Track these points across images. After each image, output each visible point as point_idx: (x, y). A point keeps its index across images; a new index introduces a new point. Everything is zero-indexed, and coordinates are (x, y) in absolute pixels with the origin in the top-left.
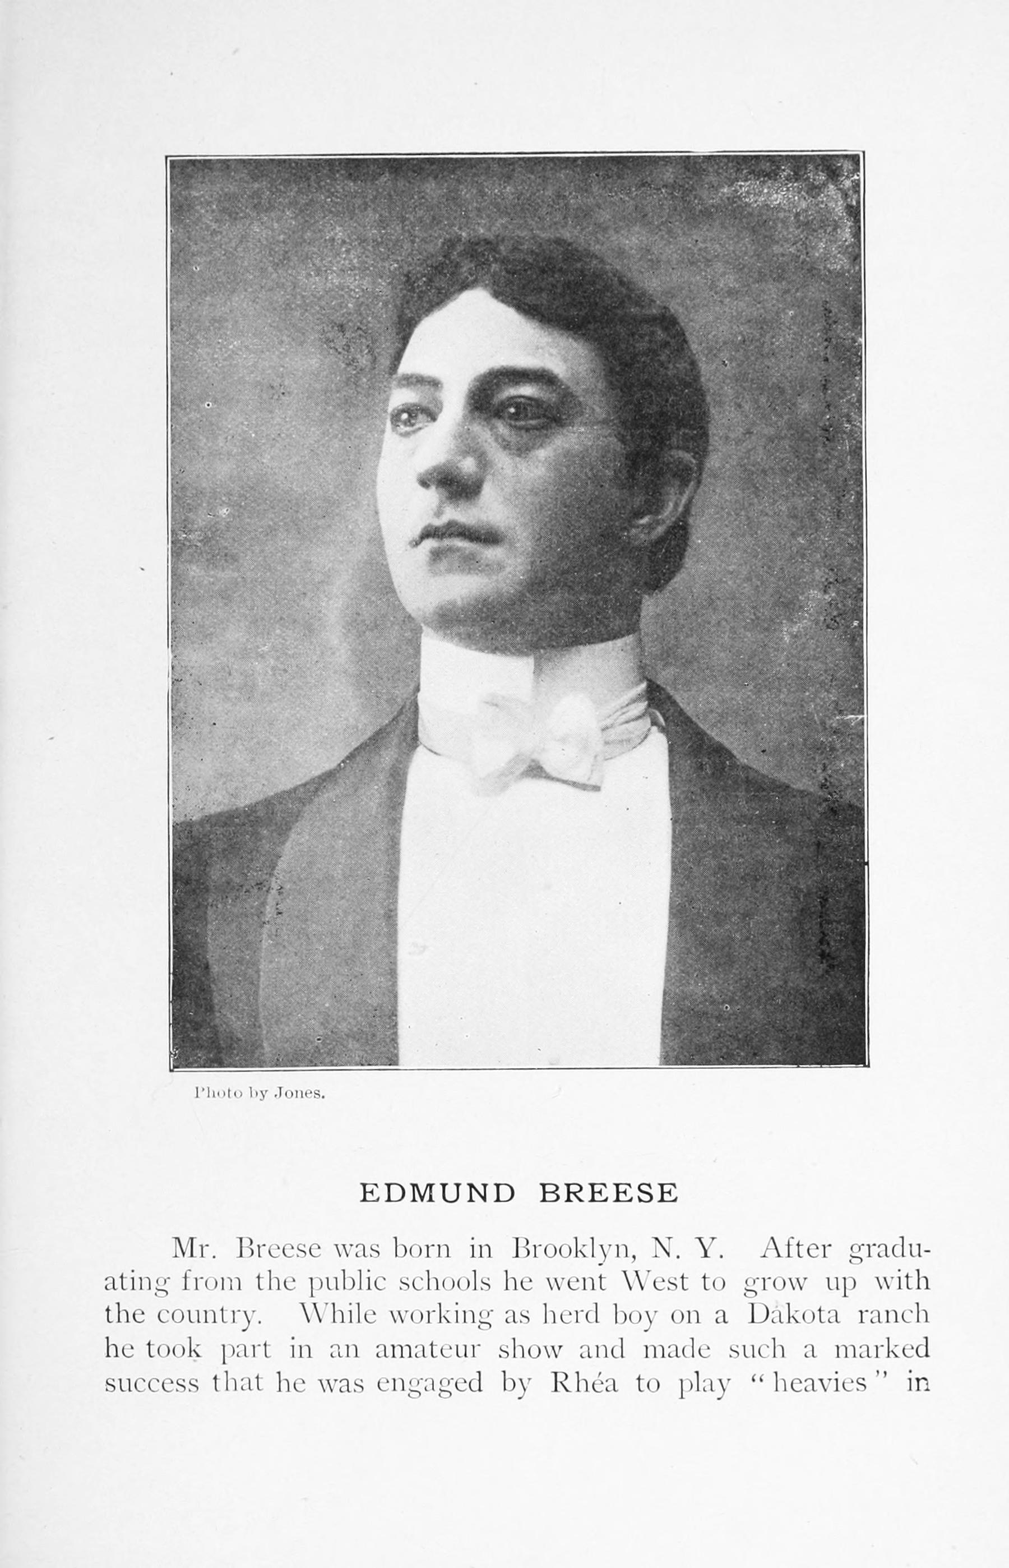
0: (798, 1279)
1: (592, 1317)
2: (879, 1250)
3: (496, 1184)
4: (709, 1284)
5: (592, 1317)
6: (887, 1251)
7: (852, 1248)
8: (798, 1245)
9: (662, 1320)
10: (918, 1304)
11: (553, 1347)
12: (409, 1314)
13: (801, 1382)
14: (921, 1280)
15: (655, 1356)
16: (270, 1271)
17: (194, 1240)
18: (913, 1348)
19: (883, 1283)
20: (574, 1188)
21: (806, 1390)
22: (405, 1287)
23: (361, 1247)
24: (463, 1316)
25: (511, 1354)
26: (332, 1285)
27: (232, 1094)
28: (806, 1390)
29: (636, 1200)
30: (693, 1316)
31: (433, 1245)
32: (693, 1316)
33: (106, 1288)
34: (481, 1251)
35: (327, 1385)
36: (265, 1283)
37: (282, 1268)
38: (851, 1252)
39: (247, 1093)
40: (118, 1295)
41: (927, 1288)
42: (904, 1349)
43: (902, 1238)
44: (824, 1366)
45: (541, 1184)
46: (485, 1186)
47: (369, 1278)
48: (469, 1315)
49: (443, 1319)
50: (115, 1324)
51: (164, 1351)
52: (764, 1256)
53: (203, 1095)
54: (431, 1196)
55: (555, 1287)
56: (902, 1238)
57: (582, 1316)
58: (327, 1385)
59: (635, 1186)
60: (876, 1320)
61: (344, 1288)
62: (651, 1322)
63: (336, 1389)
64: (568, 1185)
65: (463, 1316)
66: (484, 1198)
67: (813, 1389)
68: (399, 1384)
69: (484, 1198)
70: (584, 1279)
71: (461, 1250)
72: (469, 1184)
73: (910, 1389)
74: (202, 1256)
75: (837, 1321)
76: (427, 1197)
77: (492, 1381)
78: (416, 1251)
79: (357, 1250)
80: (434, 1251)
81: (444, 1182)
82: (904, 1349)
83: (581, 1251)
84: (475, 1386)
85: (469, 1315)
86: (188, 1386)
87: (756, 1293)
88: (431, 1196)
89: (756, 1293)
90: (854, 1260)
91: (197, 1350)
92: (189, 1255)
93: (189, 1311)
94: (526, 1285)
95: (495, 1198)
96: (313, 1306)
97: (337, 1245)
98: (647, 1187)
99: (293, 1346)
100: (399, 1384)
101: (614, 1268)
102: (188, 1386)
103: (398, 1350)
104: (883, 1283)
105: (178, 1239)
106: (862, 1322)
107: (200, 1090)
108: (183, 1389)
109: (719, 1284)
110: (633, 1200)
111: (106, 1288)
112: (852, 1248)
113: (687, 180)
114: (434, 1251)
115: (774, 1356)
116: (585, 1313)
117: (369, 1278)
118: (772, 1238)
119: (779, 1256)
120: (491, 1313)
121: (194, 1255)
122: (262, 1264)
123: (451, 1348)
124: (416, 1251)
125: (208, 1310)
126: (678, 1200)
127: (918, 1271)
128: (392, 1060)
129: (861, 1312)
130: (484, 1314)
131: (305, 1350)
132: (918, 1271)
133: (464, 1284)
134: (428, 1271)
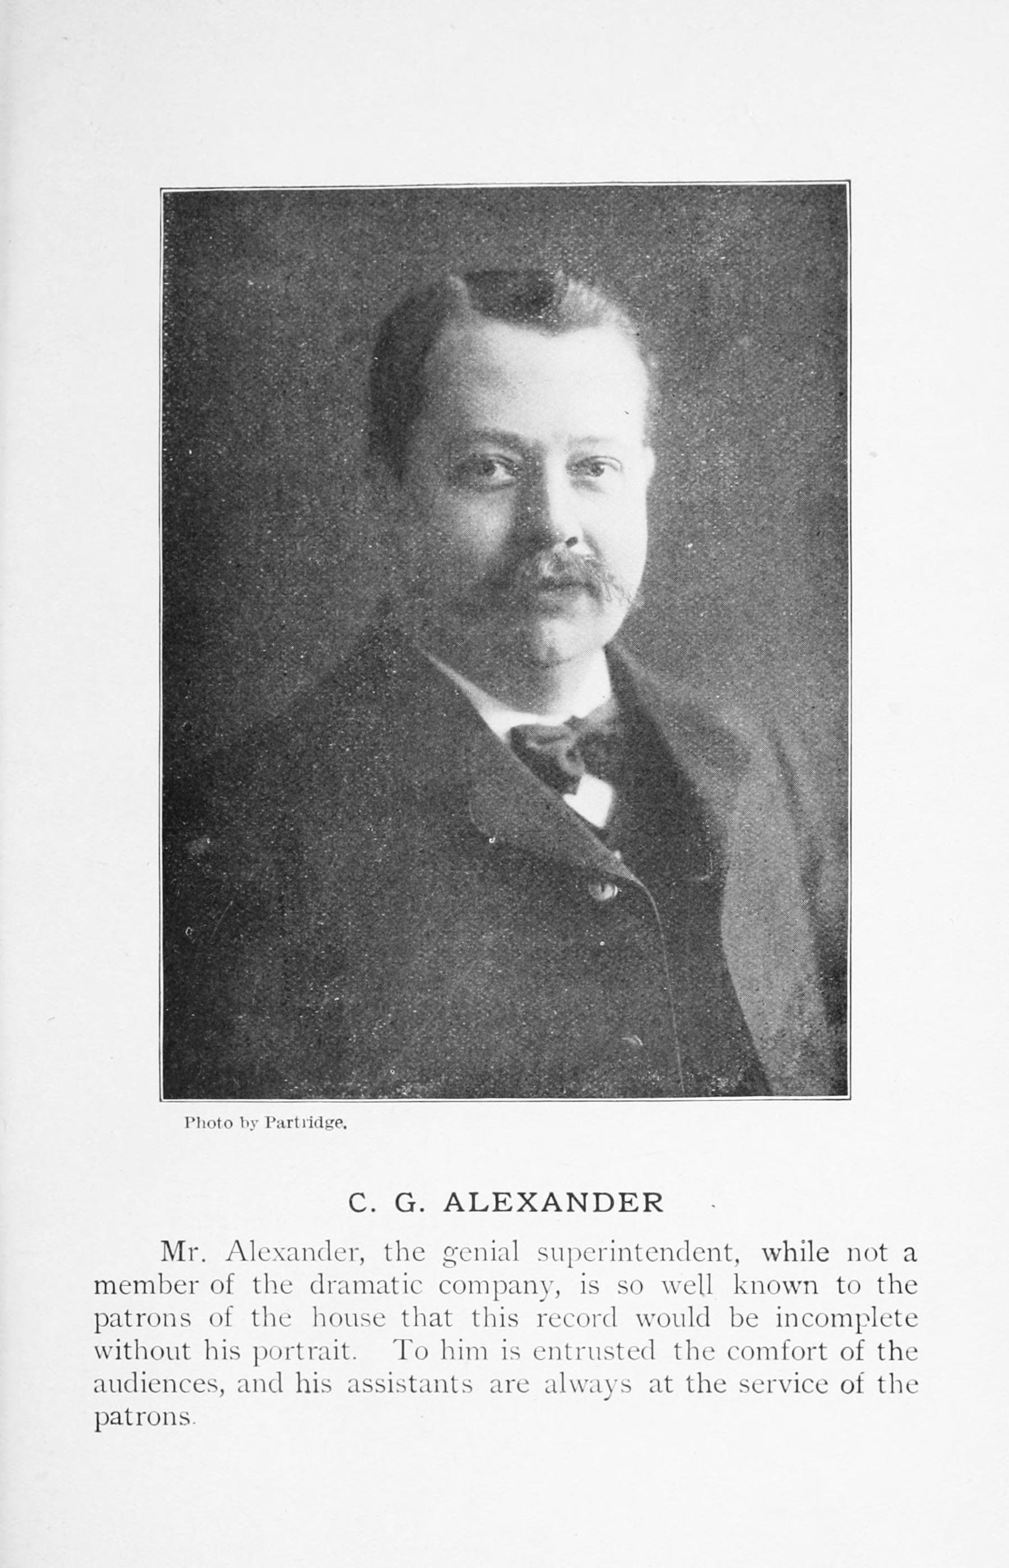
0: (672, 1282)
1: (609, 1320)
3: (595, 1194)
4: (844, 1288)
5: (609, 1320)
6: (675, 1256)
10: (265, 1307)
11: (646, 1316)
12: (656, 1318)
15: (145, 1292)
17: (183, 1244)
18: (638, 1350)
19: (670, 1287)
21: (421, 1391)
22: (623, 1290)
26: (679, 1322)
27: (222, 1123)
37: (280, 1272)
38: (444, 1256)
39: (237, 1123)
40: (263, 1299)
42: (629, 1352)
43: (687, 1242)
45: (494, 1193)
46: (585, 1195)
47: (406, 1282)
52: (229, 1260)
53: (193, 1125)
55: (671, 1291)
56: (687, 1242)
57: (599, 1320)
61: (161, 1292)
63: (587, 1390)
64: (623, 1195)
66: (584, 1208)
67: (103, 1390)
69: (584, 1208)
70: (165, 1381)
72: (568, 1194)
74: (191, 1259)
81: (584, 1192)
82: (629, 1352)
86: (375, 1387)
90: (448, 1264)
91: (743, 1287)
92: (178, 1258)
93: (675, 1315)
94: (286, 1288)
95: (595, 1208)
101: (722, 1273)
102: (375, 1387)
103: (473, 1352)
104: (670, 1287)
105: (166, 1242)
106: (403, 1358)
107: (190, 1120)
108: (369, 1388)
109: (854, 1287)
110: (513, 1209)
113: (208, 665)
115: (551, 1358)
116: (603, 1316)
117: (406, 1282)
118: (237, 1242)
119: (244, 1259)
122: (257, 1269)
125: (835, 1314)
128: (844, 1092)
129: (540, 1315)
134: (266, 1274)
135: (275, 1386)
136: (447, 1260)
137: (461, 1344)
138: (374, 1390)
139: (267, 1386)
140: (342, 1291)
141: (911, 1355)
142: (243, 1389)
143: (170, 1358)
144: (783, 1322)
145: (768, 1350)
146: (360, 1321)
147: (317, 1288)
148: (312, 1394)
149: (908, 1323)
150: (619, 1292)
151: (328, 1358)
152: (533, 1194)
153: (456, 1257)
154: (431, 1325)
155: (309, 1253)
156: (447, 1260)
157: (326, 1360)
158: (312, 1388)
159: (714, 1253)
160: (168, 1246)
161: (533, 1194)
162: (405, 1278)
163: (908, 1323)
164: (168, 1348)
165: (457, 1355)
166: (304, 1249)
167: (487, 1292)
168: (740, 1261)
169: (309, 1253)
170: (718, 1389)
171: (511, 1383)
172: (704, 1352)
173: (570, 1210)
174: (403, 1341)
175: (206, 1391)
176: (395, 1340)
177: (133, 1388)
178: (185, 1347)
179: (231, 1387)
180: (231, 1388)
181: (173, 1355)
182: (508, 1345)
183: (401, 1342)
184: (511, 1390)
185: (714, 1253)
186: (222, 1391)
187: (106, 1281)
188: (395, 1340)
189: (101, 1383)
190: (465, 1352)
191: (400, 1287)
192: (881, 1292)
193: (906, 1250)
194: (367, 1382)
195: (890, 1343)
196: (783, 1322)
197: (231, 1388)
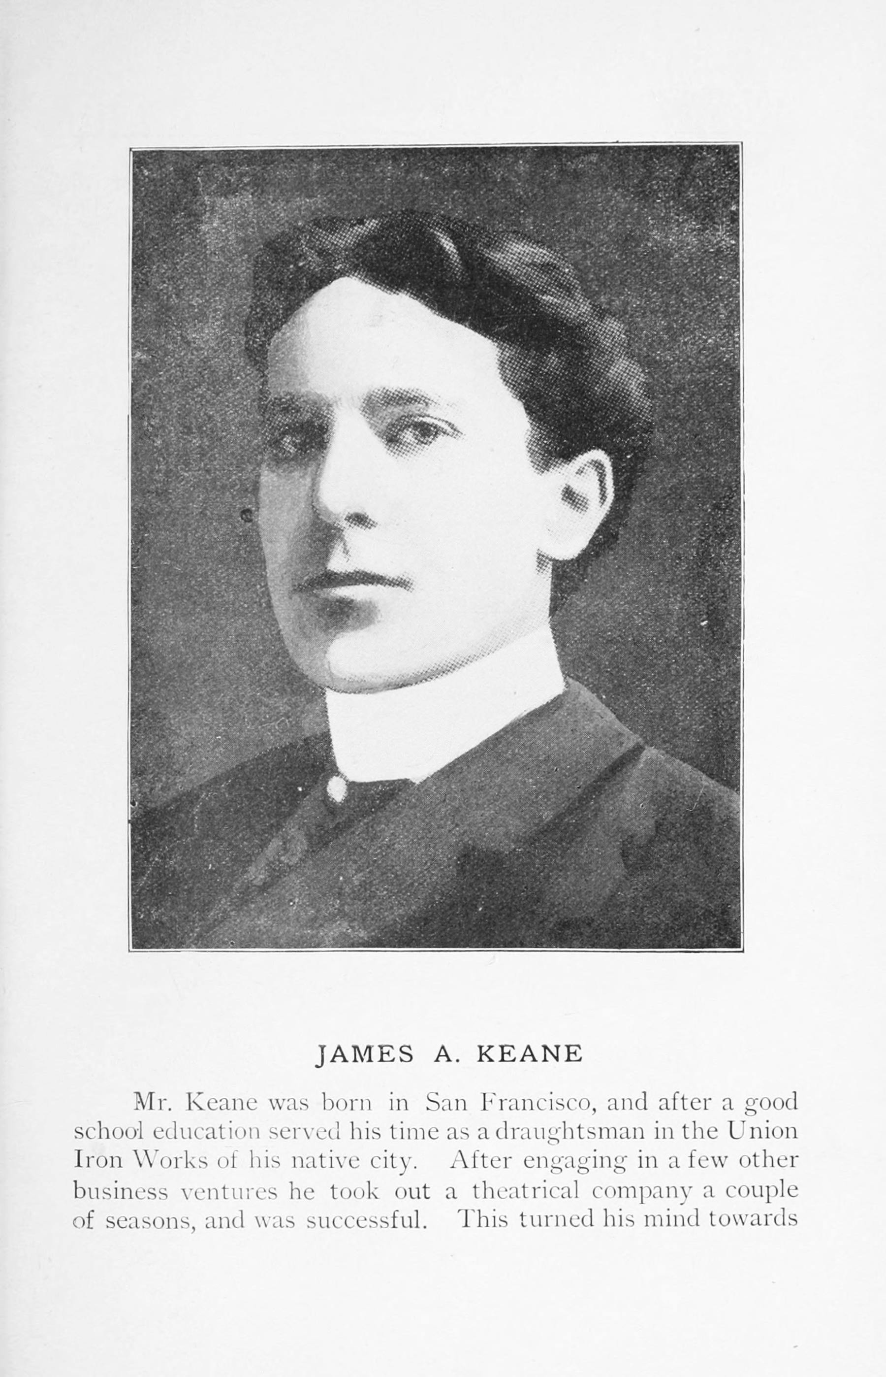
2: (510, 1104)
3: (379, 1046)
7: (747, 1102)
8: (683, 1099)
9: (516, 1164)
13: (506, 1190)
14: (102, 1131)
16: (694, 1122)
17: (153, 1095)
20: (385, 1050)
21: (130, 1227)
22: (79, 1136)
23: (292, 1101)
24: (600, 1162)
25: (113, 1195)
28: (130, 1227)
29: (397, 1060)
30: (791, 1132)
31: (357, 1100)
32: (791, 1132)
33: (449, 1138)
34: (401, 1104)
35: (262, 1222)
36: (690, 1132)
38: (746, 1105)
40: (764, 1143)
41: (642, 1138)
43: (645, 1093)
44: (723, 1206)
45: (320, 1046)
46: (557, 1047)
48: (606, 1161)
49: (189, 1165)
50: (761, 1168)
51: (346, 1193)
54: (370, 1057)
56: (645, 1093)
58: (262, 1222)
59: (397, 1048)
60: (525, 1136)
62: (406, 1167)
63: (270, 1225)
65: (600, 1162)
66: (557, 1058)
68: (543, 1161)
69: (557, 1058)
71: (381, 1104)
73: (606, 1225)
75: (314, 1166)
76: (366, 1058)
77: (249, 1221)
78: (342, 1105)
79: (289, 1103)
80: (357, 1104)
82: (700, 1160)
83: (194, 1102)
84: (587, 1221)
85: (606, 1161)
86: (158, 1195)
87: (558, 1141)
88: (370, 1057)
89: (558, 1141)
90: (749, 1112)
92: (149, 1108)
96: (144, 1153)
97: (271, 1100)
98: (408, 1049)
99: (116, 1189)
100: (543, 1161)
102: (380, 1223)
105: (138, 1093)
106: (466, 1225)
111: (449, 1138)
112: (747, 1102)
114: (357, 1104)
120: (625, 1159)
121: (153, 1108)
123: (204, 1191)
124: (342, 1105)
126: (582, 1060)
127: (100, 1122)
130: (619, 1160)
131: (651, 1161)
132: (100, 1122)
133: (131, 1133)
135: (238, 1222)
136: (748, 1110)
137: (595, 1154)
138: (379, 1226)
139: (231, 1223)
140: (209, 1136)
141: (309, 1195)
142: (210, 1225)
143: (755, 1196)
144: (644, 1164)
145: (608, 1130)
146: (597, 1132)
147: (502, 1134)
148: (414, 1229)
149: (350, 1165)
150: (76, 1137)
151: (660, 1196)
152: (490, 1047)
153: (756, 1107)
154: (307, 1167)
155: (238, 1103)
156: (748, 1110)
157: (711, 1198)
158: (491, 1223)
159: (213, 1193)
160: (140, 1096)
161: (490, 1047)
162: (231, 1125)
163: (350, 1165)
164: (410, 1189)
165: (665, 1222)
166: (160, 1100)
167: (258, 1137)
168: (597, 1110)
169: (238, 1103)
170: (360, 1225)
171: (769, 1218)
172: (305, 1192)
173: (545, 1060)
174: (466, 1211)
175: (368, 1226)
176: (459, 1210)
177: (240, 1225)
178: (425, 1187)
179: (199, 1222)
180: (200, 1225)
181: (415, 1194)
182: (118, 1185)
183: (464, 1212)
184: (768, 1223)
185: (213, 1193)
186: (194, 1228)
187: (609, 1128)
188: (459, 1210)
189: (757, 1217)
190: (120, 1192)
191: (226, 1133)
192: (686, 1138)
193: (724, 1100)
194: (146, 1220)
195: (74, 1183)
196: (644, 1164)
197: (200, 1225)
